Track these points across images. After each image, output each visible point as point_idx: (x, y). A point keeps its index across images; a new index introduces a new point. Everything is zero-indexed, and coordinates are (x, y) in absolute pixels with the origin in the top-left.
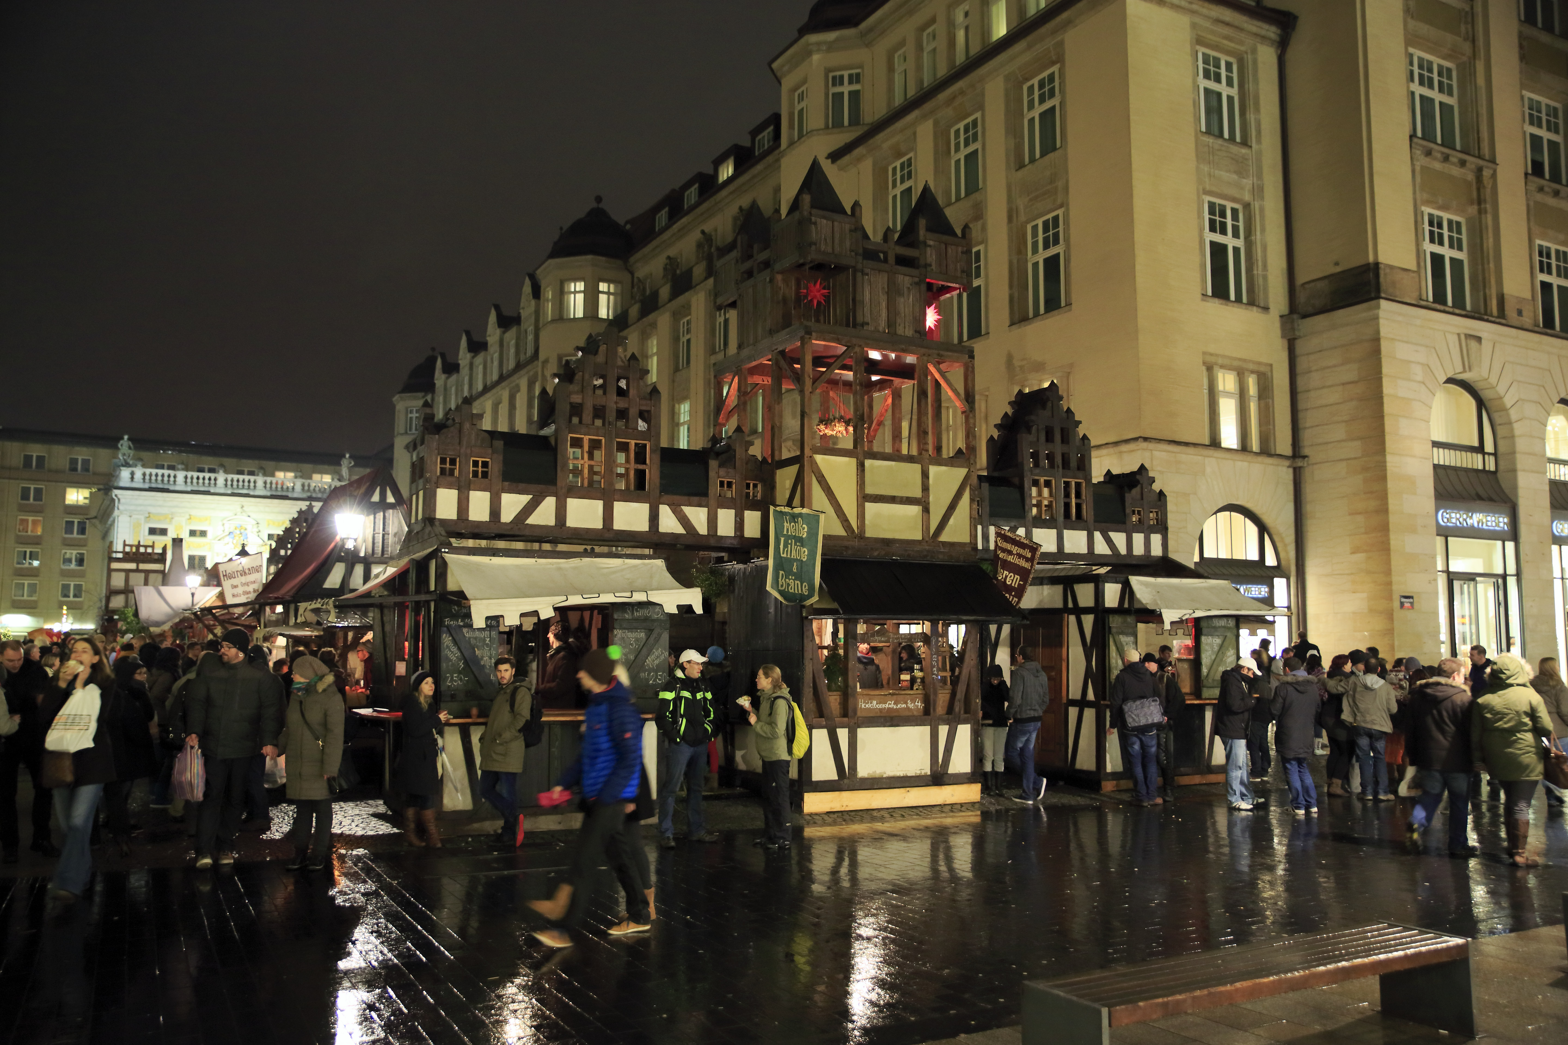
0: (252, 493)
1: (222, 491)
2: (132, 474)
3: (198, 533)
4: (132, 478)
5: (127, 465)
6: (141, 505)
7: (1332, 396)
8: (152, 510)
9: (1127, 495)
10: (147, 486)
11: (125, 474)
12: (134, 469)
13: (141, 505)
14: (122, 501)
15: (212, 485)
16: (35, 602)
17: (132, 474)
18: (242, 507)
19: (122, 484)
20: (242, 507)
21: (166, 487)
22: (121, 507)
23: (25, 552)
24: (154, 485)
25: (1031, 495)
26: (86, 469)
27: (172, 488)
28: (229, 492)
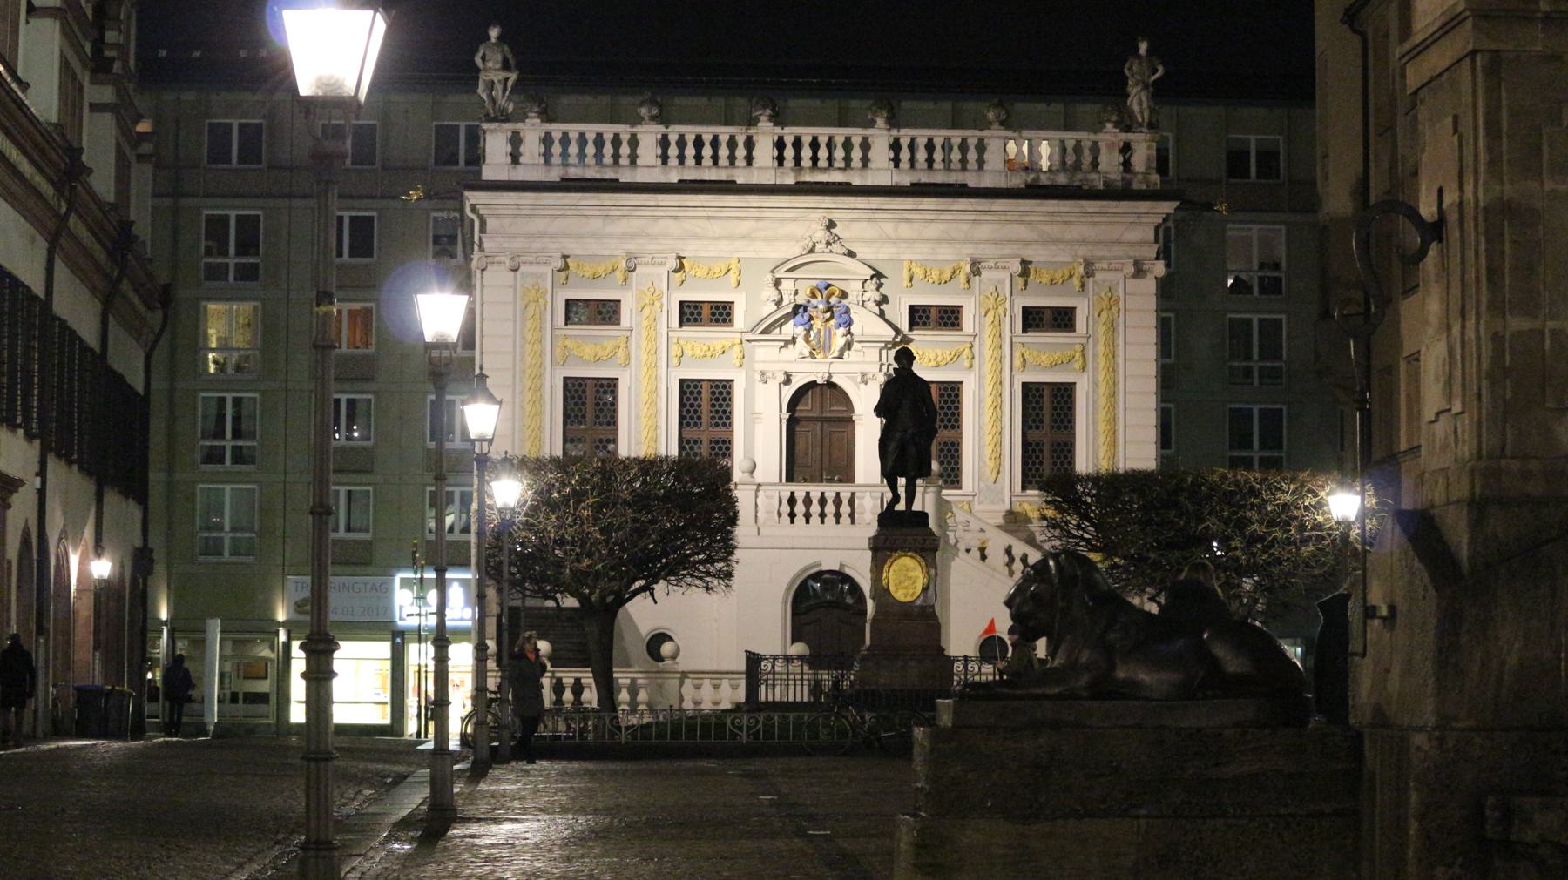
0: (856, 180)
1: (768, 178)
2: (516, 140)
3: (706, 311)
4: (515, 158)
5: (502, 117)
6: (541, 235)
7: (85, 235)
8: (572, 247)
9: (742, 699)
10: (554, 175)
11: (496, 144)
12: (519, 126)
13: (541, 235)
14: (491, 223)
15: (740, 162)
16: (367, 546)
17: (516, 140)
18: (831, 225)
19: (488, 174)
20: (831, 225)
21: (609, 174)
22: (487, 245)
23: (222, 401)
24: (574, 172)
25: (481, 651)
26: (250, 152)
27: (625, 176)
28: (790, 180)
